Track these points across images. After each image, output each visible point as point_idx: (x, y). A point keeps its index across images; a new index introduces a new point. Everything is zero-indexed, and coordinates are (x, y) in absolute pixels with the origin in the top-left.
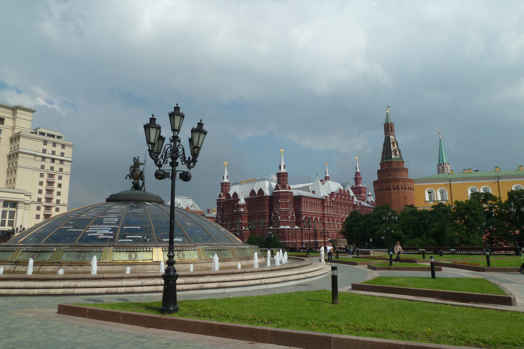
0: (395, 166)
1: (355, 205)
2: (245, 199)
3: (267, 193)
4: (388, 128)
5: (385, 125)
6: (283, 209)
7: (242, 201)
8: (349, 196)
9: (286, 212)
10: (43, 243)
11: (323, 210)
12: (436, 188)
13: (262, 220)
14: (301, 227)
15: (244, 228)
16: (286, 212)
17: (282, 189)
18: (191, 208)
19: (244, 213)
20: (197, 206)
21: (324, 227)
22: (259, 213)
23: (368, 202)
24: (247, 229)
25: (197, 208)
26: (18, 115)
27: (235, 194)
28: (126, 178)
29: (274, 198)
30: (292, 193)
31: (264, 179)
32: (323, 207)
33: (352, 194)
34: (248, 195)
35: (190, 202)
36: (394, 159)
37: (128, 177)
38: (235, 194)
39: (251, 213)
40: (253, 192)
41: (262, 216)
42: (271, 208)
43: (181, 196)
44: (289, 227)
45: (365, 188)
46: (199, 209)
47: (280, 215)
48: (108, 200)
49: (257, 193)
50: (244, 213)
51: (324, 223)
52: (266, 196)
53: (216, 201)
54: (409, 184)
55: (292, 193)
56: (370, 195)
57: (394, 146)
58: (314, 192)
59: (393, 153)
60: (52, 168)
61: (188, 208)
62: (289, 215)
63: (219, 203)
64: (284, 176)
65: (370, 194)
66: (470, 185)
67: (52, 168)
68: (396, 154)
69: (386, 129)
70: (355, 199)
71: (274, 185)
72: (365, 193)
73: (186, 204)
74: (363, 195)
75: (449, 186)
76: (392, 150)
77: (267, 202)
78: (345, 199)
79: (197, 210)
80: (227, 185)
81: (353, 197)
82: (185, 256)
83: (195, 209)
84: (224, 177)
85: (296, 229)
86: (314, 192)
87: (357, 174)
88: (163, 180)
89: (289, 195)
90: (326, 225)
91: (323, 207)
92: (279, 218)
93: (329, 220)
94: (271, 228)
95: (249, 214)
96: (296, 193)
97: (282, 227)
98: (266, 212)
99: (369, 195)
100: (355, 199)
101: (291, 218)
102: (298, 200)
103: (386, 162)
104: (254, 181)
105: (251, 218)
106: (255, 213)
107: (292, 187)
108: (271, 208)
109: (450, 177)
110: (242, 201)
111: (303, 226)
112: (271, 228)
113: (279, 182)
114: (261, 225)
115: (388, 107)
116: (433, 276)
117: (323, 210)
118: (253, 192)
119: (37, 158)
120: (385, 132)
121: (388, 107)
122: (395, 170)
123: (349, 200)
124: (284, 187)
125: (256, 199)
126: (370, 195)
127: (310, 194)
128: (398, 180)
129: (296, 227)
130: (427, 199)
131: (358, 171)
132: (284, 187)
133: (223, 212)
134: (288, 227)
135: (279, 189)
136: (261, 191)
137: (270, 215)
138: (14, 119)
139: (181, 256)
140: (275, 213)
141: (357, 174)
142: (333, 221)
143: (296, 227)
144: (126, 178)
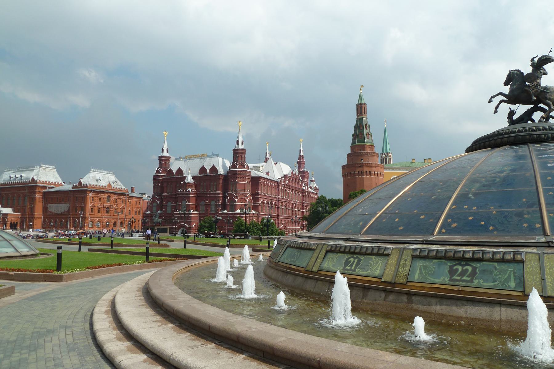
0: (367, 150)
1: (303, 190)
2: (193, 178)
3: (221, 171)
4: (361, 109)
5: (357, 105)
7: (189, 180)
9: (244, 194)
10: (366, 233)
11: (278, 193)
13: (213, 202)
14: (258, 211)
15: (192, 211)
16: (244, 194)
17: (239, 167)
18: (113, 185)
19: (192, 194)
20: (120, 183)
21: (278, 212)
22: (210, 194)
24: (195, 212)
25: (120, 186)
27: (180, 171)
29: (229, 179)
30: (250, 172)
31: (217, 156)
32: (278, 190)
34: (196, 173)
35: (112, 178)
36: (367, 142)
38: (180, 171)
39: (200, 194)
40: (203, 170)
41: (215, 197)
42: (225, 190)
43: (101, 170)
45: (308, 173)
46: (123, 187)
47: (237, 198)
48: (469, 150)
49: (208, 171)
50: (192, 194)
51: (278, 208)
52: (220, 175)
54: (374, 170)
55: (250, 172)
56: (314, 181)
57: (366, 129)
58: (267, 173)
59: (365, 136)
61: (109, 185)
62: (247, 197)
63: (156, 180)
64: (242, 153)
65: (313, 179)
68: (368, 138)
69: (359, 109)
71: (228, 164)
72: (308, 178)
73: (107, 179)
74: (306, 180)
76: (365, 133)
77: (221, 182)
78: (295, 183)
79: (120, 187)
80: (166, 160)
83: (118, 187)
84: (163, 150)
85: (253, 214)
87: (301, 157)
88: (507, 120)
89: (246, 175)
90: (280, 211)
91: (278, 190)
92: (236, 200)
93: (282, 205)
94: (225, 211)
95: (198, 194)
96: (254, 173)
98: (219, 194)
99: (312, 181)
101: (249, 201)
102: (255, 181)
103: (358, 145)
104: (204, 156)
105: (199, 199)
106: (205, 194)
107: (250, 166)
108: (225, 190)
110: (189, 180)
111: (260, 211)
112: (225, 211)
113: (236, 159)
114: (213, 208)
115: (362, 86)
116: (80, 250)
117: (278, 193)
118: (203, 170)
120: (358, 113)
121: (362, 86)
122: (367, 155)
124: (243, 166)
125: (206, 178)
126: (314, 181)
128: (370, 165)
129: (253, 212)
131: (302, 154)
132: (243, 166)
133: (162, 191)
135: (237, 168)
136: (214, 169)
137: (224, 197)
140: (231, 195)
141: (301, 157)
142: (285, 206)
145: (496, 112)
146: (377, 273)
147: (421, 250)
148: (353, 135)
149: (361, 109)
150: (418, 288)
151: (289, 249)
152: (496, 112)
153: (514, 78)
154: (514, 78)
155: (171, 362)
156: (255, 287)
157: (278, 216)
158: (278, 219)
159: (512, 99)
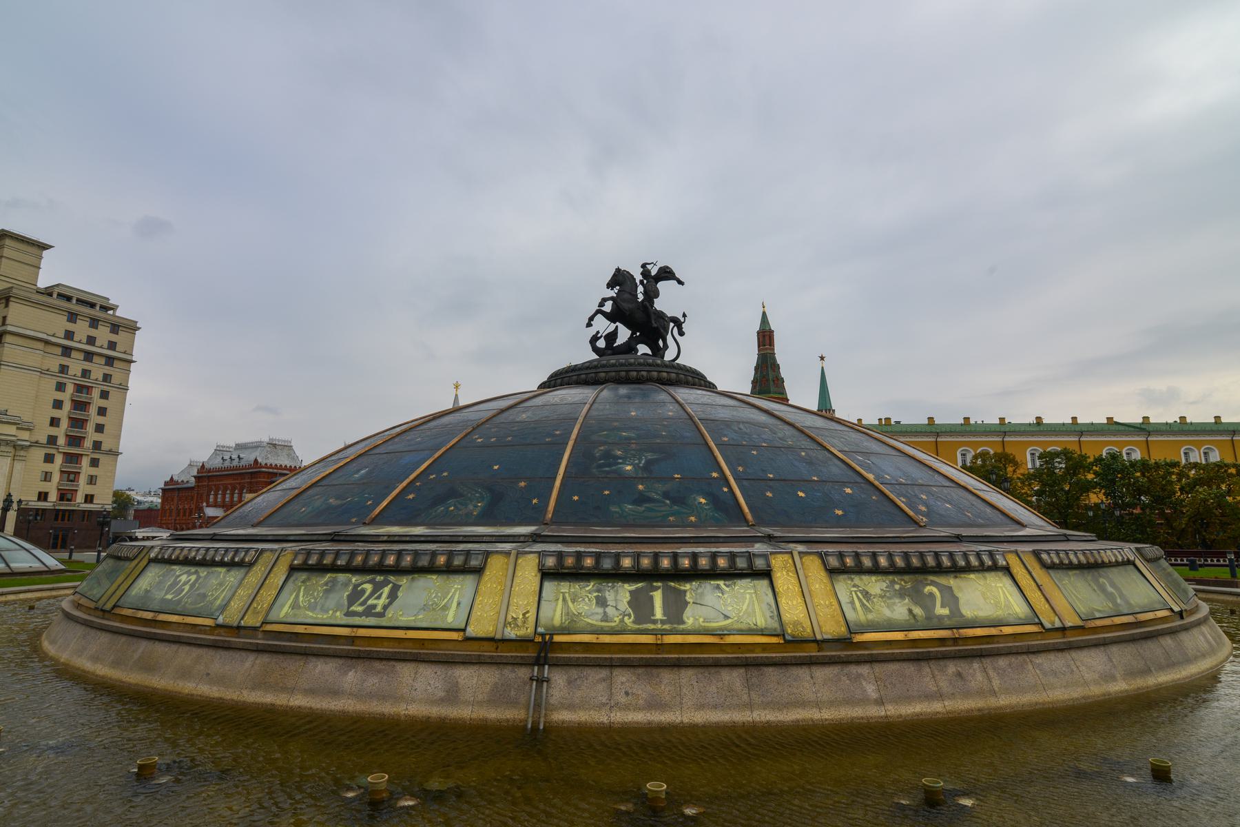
4: (765, 337)
60: (85, 373)
75: (1145, 445)
146: (452, 617)
149: (765, 337)
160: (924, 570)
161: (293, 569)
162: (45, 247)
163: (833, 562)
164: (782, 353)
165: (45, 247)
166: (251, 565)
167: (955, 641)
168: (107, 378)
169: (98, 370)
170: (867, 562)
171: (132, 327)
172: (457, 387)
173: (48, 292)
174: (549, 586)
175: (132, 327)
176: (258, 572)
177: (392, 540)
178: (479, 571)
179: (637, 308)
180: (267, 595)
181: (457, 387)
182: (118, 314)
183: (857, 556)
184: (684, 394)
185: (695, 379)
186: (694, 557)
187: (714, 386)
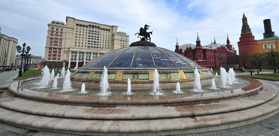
2: (185, 51)
4: (244, 20)
6: (199, 54)
8: (225, 49)
9: (200, 55)
12: (269, 43)
16: (200, 55)
23: (233, 51)
26: (113, 28)
28: (138, 37)
33: (226, 48)
34: (185, 49)
37: (138, 35)
44: (202, 60)
53: (237, 43)
55: (202, 48)
60: (124, 44)
66: (264, 43)
67: (124, 44)
69: (39, 100)
70: (228, 50)
74: (231, 48)
75: (276, 43)
81: (227, 49)
82: (172, 77)
86: (211, 48)
97: (199, 60)
100: (228, 50)
109: (276, 38)
117: (215, 54)
119: (119, 41)
123: (225, 50)
127: (210, 48)
129: (204, 60)
130: (264, 48)
134: (201, 60)
138: (112, 30)
139: (169, 77)
143: (204, 60)
144: (138, 37)
145: (135, 35)
146: (113, 78)
147: (97, 71)
148: (242, 30)
149: (244, 20)
150: (167, 82)
151: (77, 73)
152: (135, 35)
153: (141, 29)
154: (141, 29)
155: (27, 97)
156: (57, 82)
157: (215, 61)
158: (215, 62)
159: (140, 34)
160: (167, 73)
161: (95, 73)
162: (117, 27)
163: (184, 72)
164: (249, 23)
165: (117, 27)
166: (89, 73)
167: (135, 81)
168: (126, 44)
169: (125, 43)
170: (176, 72)
171: (128, 36)
172: (177, 39)
173: (118, 33)
174: (124, 74)
175: (128, 36)
176: (90, 74)
177: (167, 69)
178: (116, 73)
179: (144, 32)
180: (92, 76)
181: (177, 39)
182: (127, 34)
183: (173, 71)
184: (151, 48)
185: (153, 45)
186: (170, 71)
187: (156, 46)
